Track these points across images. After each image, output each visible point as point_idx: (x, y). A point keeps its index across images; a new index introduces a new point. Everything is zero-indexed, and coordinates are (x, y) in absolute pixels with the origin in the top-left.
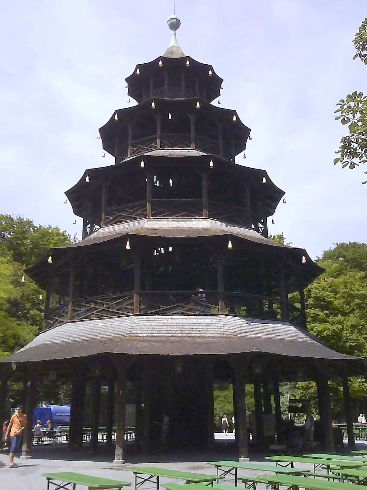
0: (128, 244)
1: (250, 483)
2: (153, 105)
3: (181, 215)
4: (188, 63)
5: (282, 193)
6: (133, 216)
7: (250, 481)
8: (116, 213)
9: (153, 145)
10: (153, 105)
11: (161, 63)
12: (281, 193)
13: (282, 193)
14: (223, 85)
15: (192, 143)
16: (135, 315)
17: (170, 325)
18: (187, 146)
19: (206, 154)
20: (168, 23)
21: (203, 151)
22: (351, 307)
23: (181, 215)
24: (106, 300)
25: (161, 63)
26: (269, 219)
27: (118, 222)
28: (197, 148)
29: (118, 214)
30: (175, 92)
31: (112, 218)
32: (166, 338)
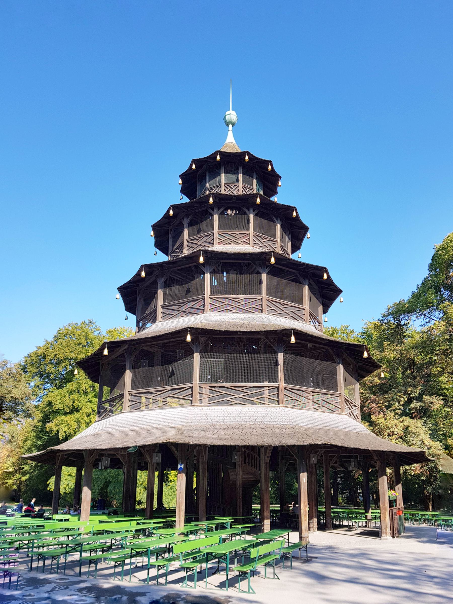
4: (247, 158)
11: (218, 157)
25: (218, 157)
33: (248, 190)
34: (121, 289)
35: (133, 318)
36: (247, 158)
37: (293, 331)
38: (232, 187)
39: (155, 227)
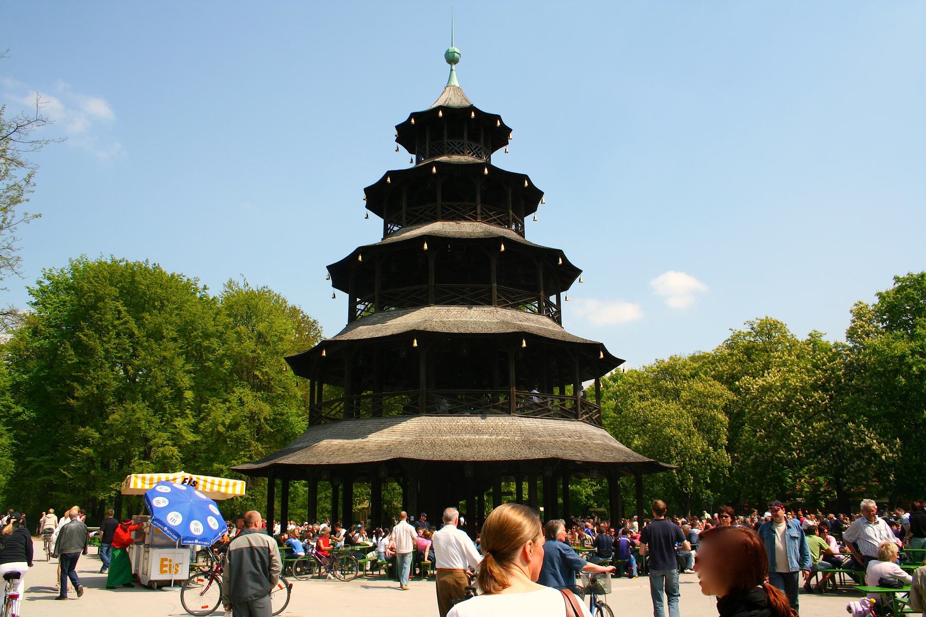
11: (441, 114)
14: (511, 136)
25: (441, 114)
26: (563, 294)
33: (474, 147)
38: (456, 144)
39: (398, 127)
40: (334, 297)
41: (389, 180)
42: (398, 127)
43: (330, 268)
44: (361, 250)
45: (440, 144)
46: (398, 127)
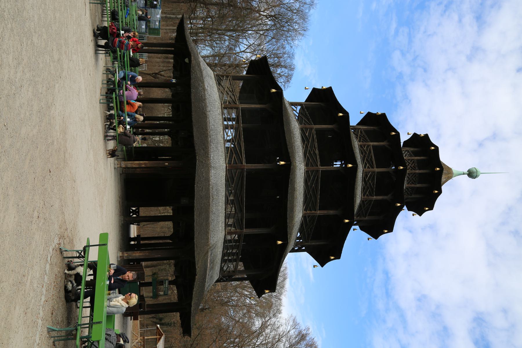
0: (303, 248)
1: (82, 254)
2: (402, 168)
3: (306, 195)
4: (436, 192)
5: (322, 265)
6: (307, 154)
7: (84, 254)
8: (311, 139)
9: (368, 165)
10: (402, 168)
12: (322, 264)
13: (322, 265)
15: (388, 143)
16: (226, 165)
17: (216, 201)
18: (364, 191)
19: (355, 214)
20: (474, 169)
21: (360, 206)
22: (229, 26)
23: (306, 195)
24: (239, 140)
27: (303, 141)
28: (363, 202)
29: (310, 141)
30: (413, 179)
31: (307, 135)
32: (207, 197)
34: (330, 90)
35: (303, 97)
36: (436, 192)
37: (286, 242)
39: (384, 116)
40: (306, 89)
41: (433, 148)
42: (426, 136)
43: (330, 90)
44: (437, 148)
45: (415, 182)
46: (426, 136)
